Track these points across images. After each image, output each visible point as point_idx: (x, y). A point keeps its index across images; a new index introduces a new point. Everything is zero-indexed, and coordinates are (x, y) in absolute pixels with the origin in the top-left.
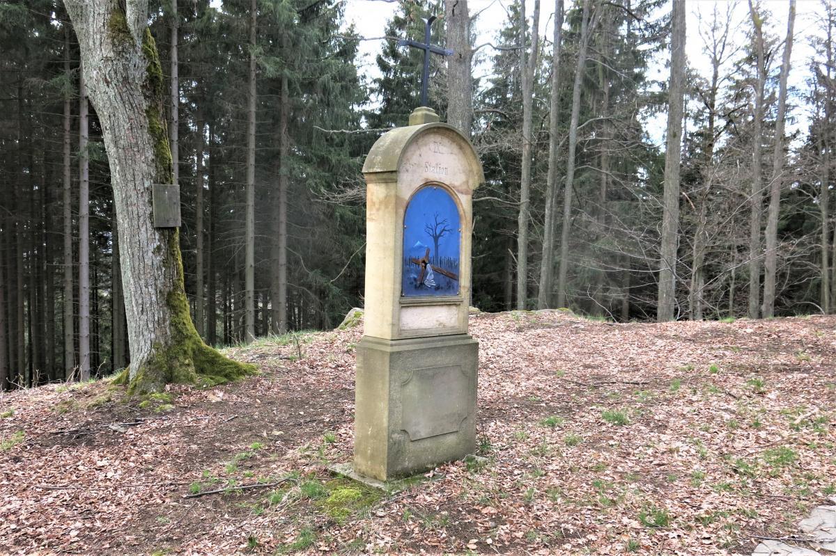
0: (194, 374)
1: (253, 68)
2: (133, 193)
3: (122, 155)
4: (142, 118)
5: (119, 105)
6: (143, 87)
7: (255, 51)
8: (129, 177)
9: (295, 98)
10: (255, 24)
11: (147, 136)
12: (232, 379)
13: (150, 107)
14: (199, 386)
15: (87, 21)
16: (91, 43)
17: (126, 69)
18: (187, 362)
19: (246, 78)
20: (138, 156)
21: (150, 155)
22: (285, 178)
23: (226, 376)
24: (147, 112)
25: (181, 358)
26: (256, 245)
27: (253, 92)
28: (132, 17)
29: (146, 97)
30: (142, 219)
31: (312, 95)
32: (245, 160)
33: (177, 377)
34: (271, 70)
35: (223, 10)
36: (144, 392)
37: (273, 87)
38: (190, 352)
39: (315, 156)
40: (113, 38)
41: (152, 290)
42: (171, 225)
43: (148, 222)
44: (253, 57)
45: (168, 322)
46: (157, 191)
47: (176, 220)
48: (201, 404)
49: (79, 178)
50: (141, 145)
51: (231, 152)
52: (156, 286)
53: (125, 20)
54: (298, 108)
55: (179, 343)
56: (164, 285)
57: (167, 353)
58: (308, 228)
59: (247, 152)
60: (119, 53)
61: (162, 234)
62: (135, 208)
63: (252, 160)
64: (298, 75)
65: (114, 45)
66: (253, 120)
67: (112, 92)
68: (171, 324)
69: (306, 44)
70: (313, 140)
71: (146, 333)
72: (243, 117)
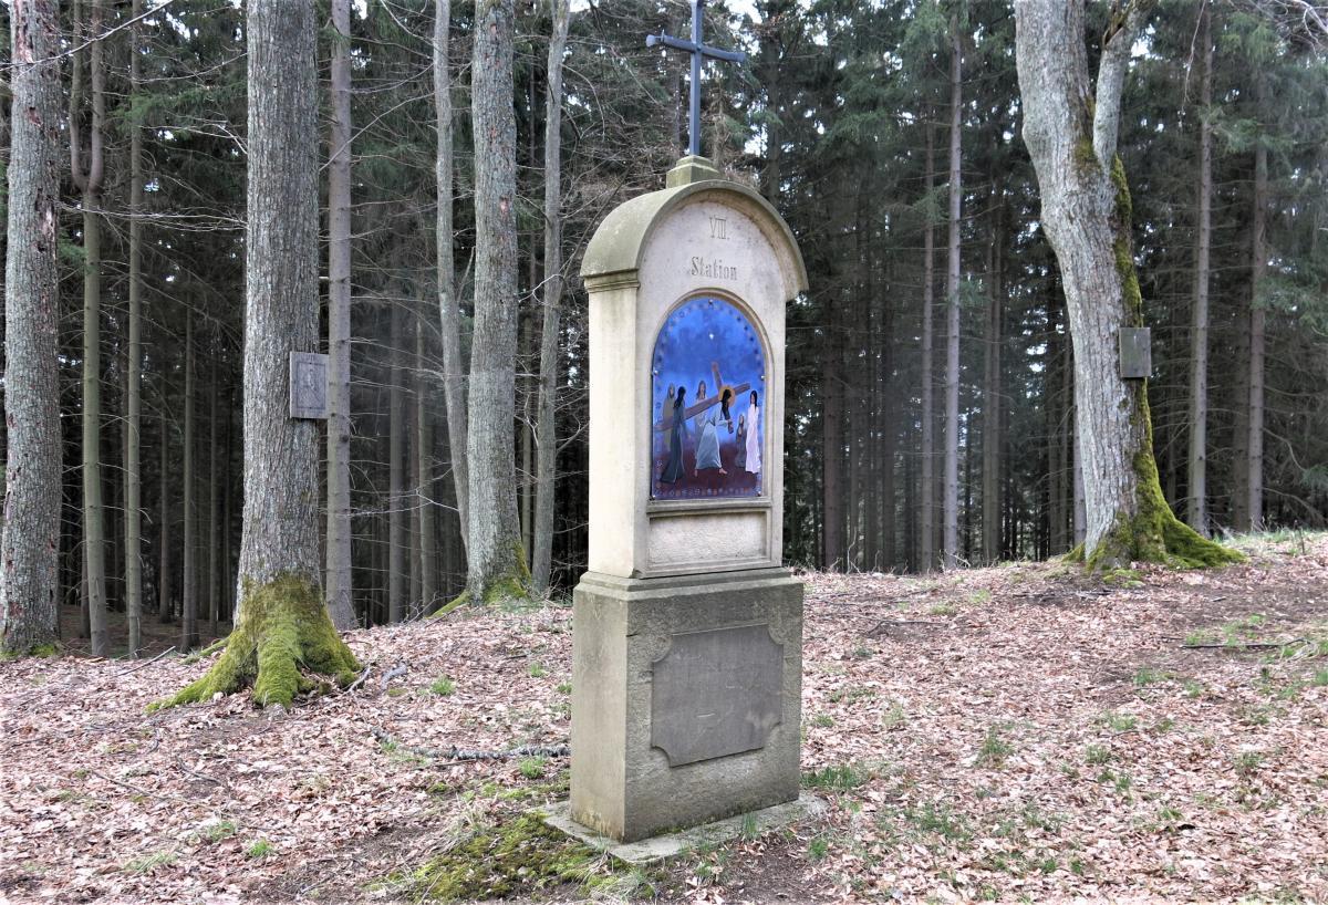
0: (1165, 553)
1: (1205, 142)
2: (1097, 341)
3: (1085, 298)
4: (1108, 255)
5: (1083, 242)
6: (1110, 219)
7: (1209, 117)
8: (1093, 322)
9: (1280, 180)
10: (1209, 71)
11: (1113, 274)
12: (1212, 565)
13: (1117, 240)
14: (1171, 567)
15: (1050, 155)
16: (1053, 178)
17: (1092, 201)
18: (1156, 537)
19: (1192, 156)
20: (1103, 298)
21: (1117, 295)
22: (1263, 313)
23: (1204, 560)
24: (1114, 246)
25: (1149, 532)
26: (1209, 426)
27: (1206, 180)
28: (1101, 144)
29: (1113, 229)
30: (1106, 369)
31: (1311, 170)
32: (1187, 289)
33: (1144, 554)
34: (1235, 139)
35: (1151, 52)
36: (1105, 568)
37: (1238, 169)
38: (1160, 527)
39: (1317, 273)
40: (1079, 169)
41: (1116, 451)
42: (1140, 375)
43: (1113, 371)
44: (1206, 125)
45: (1134, 489)
46: (1125, 336)
47: (1145, 369)
48: (1175, 584)
49: (946, 332)
50: (1107, 285)
51: (1166, 279)
52: (1121, 445)
53: (1091, 148)
54: (1285, 197)
55: (1147, 514)
56: (1131, 445)
57: (1133, 524)
58: (1304, 394)
59: (1192, 277)
60: (1084, 186)
61: (1129, 386)
62: (1098, 357)
63: (1203, 288)
64: (1287, 142)
65: (1080, 177)
66: (1206, 224)
67: (1075, 229)
68: (1138, 492)
69: (1300, 89)
70: (1314, 248)
71: (1108, 501)
72: (1187, 221)
